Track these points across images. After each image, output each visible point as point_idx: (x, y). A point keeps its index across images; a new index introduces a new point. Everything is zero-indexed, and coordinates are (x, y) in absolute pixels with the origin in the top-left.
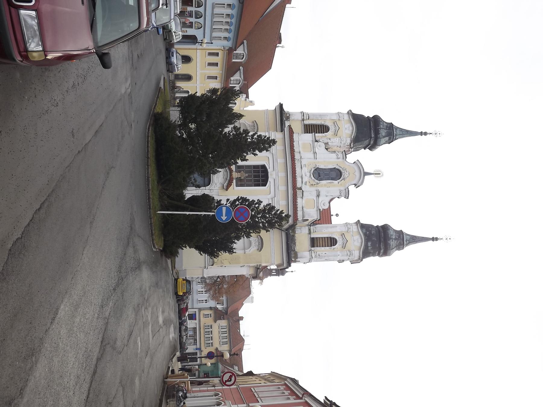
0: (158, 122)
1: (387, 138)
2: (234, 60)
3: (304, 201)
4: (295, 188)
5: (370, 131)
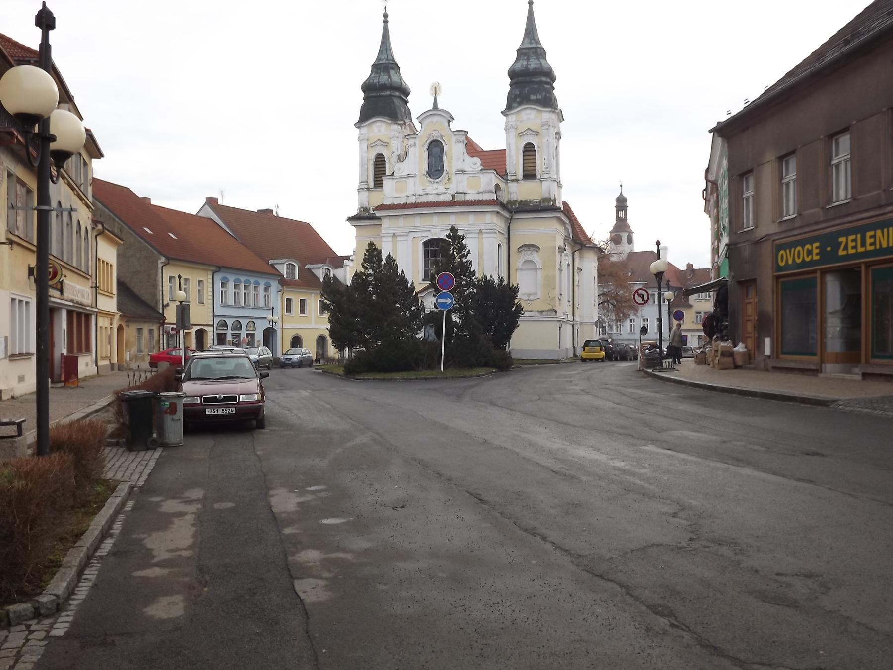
0: (353, 370)
1: (392, 72)
2: (297, 278)
3: (471, 191)
4: (452, 203)
5: (383, 96)
